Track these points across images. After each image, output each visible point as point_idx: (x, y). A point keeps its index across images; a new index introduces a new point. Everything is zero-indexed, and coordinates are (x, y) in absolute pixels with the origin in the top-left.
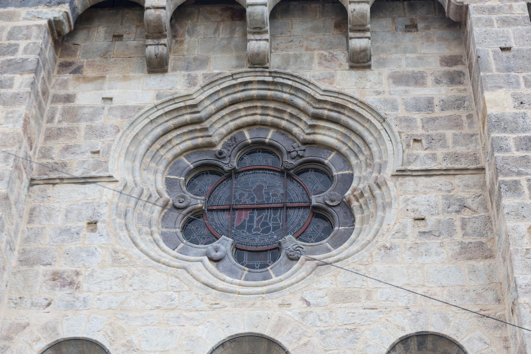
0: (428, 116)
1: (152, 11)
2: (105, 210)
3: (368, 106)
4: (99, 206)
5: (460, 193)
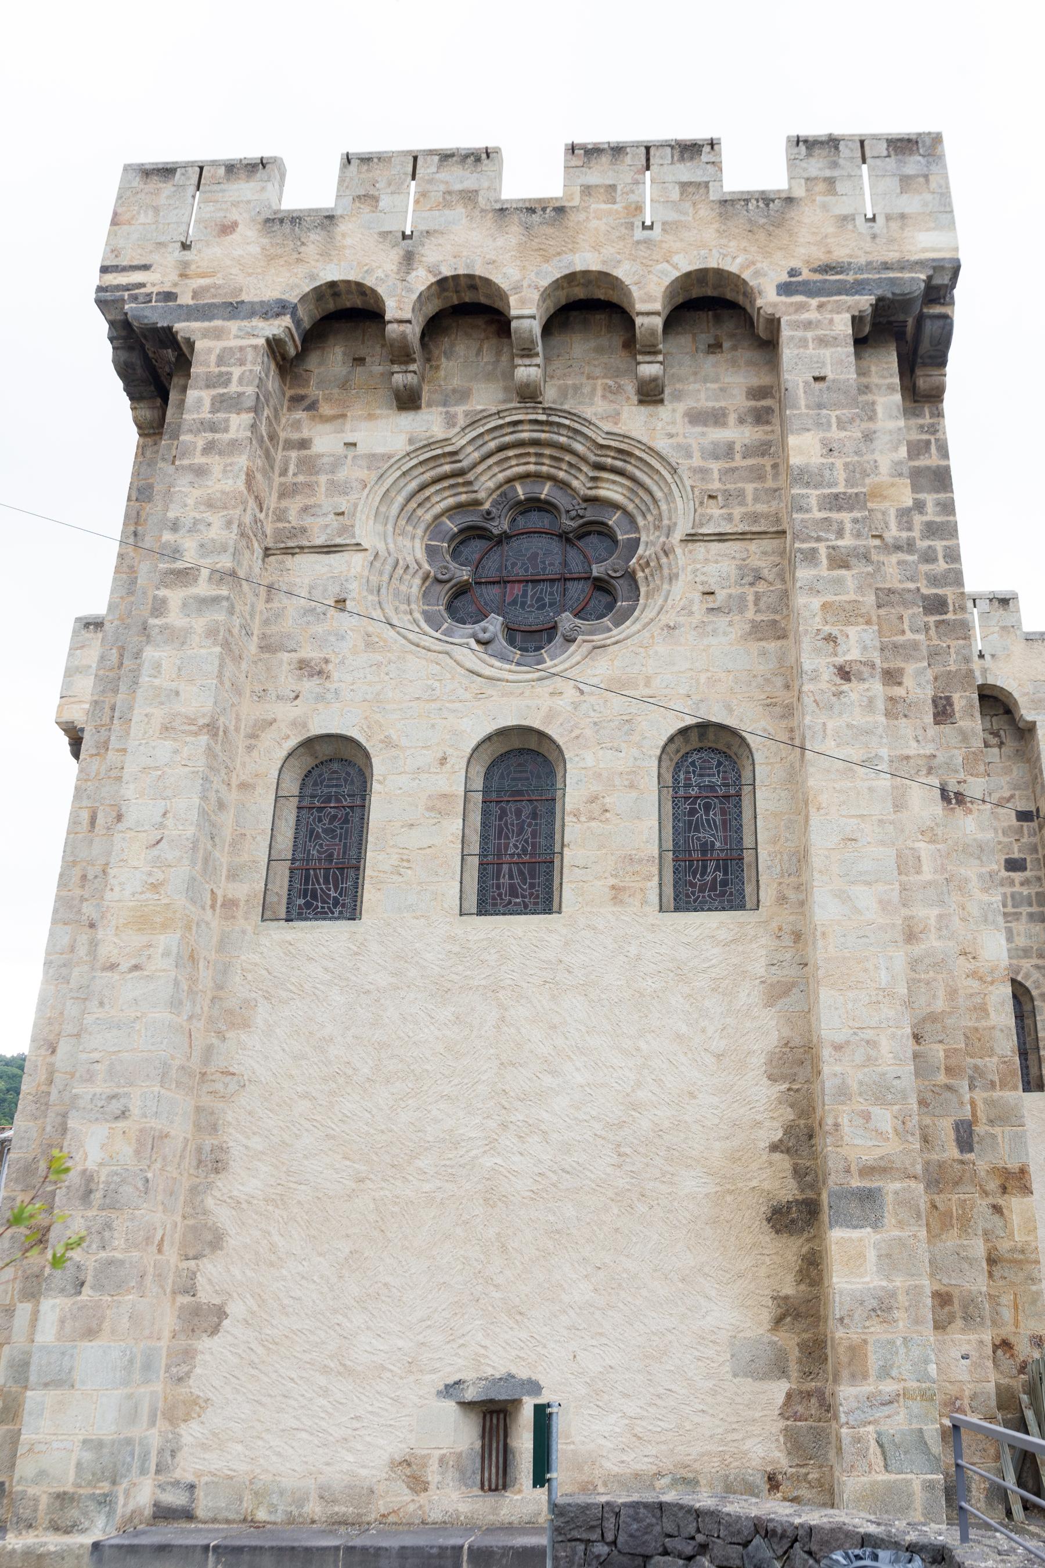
0: (727, 466)
1: (395, 326)
2: (354, 586)
3: (658, 454)
4: (346, 580)
5: (756, 562)
